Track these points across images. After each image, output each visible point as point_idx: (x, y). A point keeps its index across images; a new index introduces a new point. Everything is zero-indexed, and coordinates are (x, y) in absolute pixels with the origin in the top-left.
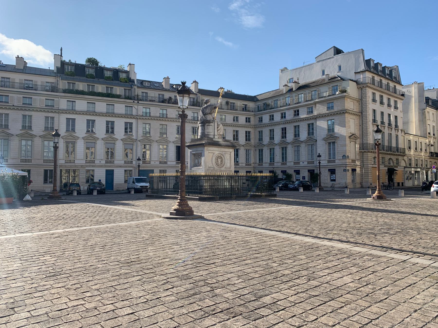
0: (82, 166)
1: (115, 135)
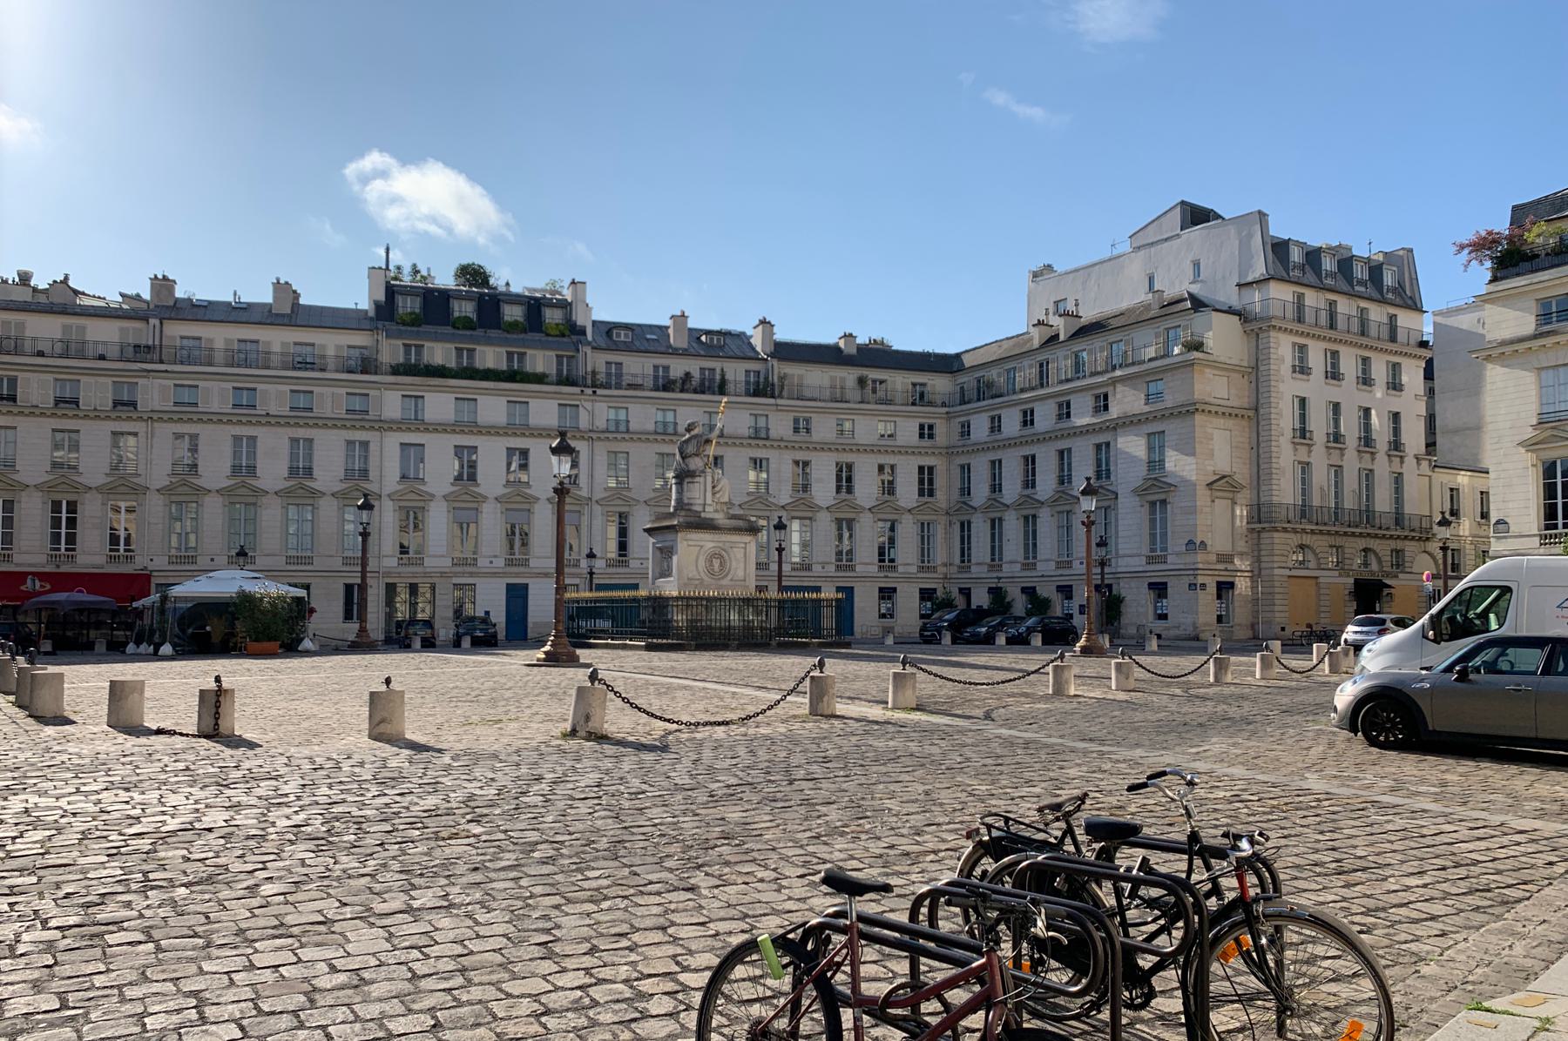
0: (443, 575)
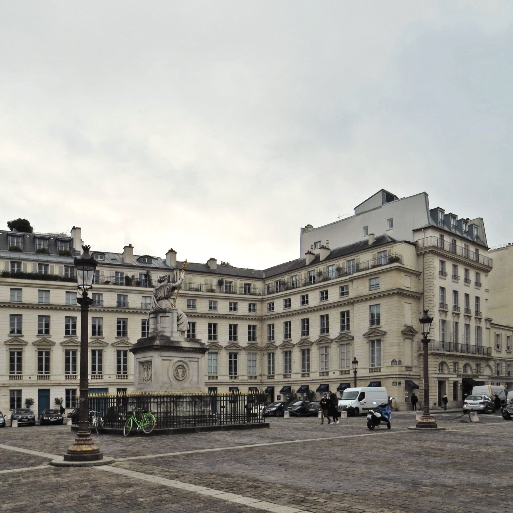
1: (50, 337)
